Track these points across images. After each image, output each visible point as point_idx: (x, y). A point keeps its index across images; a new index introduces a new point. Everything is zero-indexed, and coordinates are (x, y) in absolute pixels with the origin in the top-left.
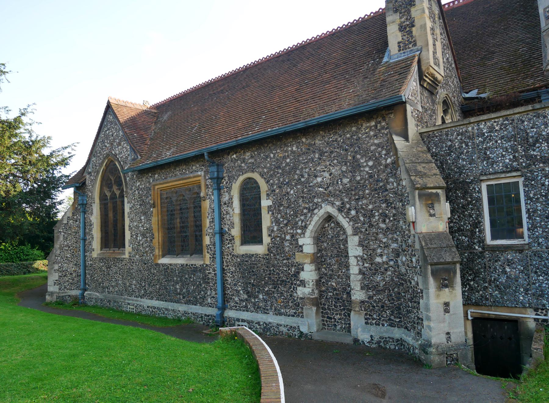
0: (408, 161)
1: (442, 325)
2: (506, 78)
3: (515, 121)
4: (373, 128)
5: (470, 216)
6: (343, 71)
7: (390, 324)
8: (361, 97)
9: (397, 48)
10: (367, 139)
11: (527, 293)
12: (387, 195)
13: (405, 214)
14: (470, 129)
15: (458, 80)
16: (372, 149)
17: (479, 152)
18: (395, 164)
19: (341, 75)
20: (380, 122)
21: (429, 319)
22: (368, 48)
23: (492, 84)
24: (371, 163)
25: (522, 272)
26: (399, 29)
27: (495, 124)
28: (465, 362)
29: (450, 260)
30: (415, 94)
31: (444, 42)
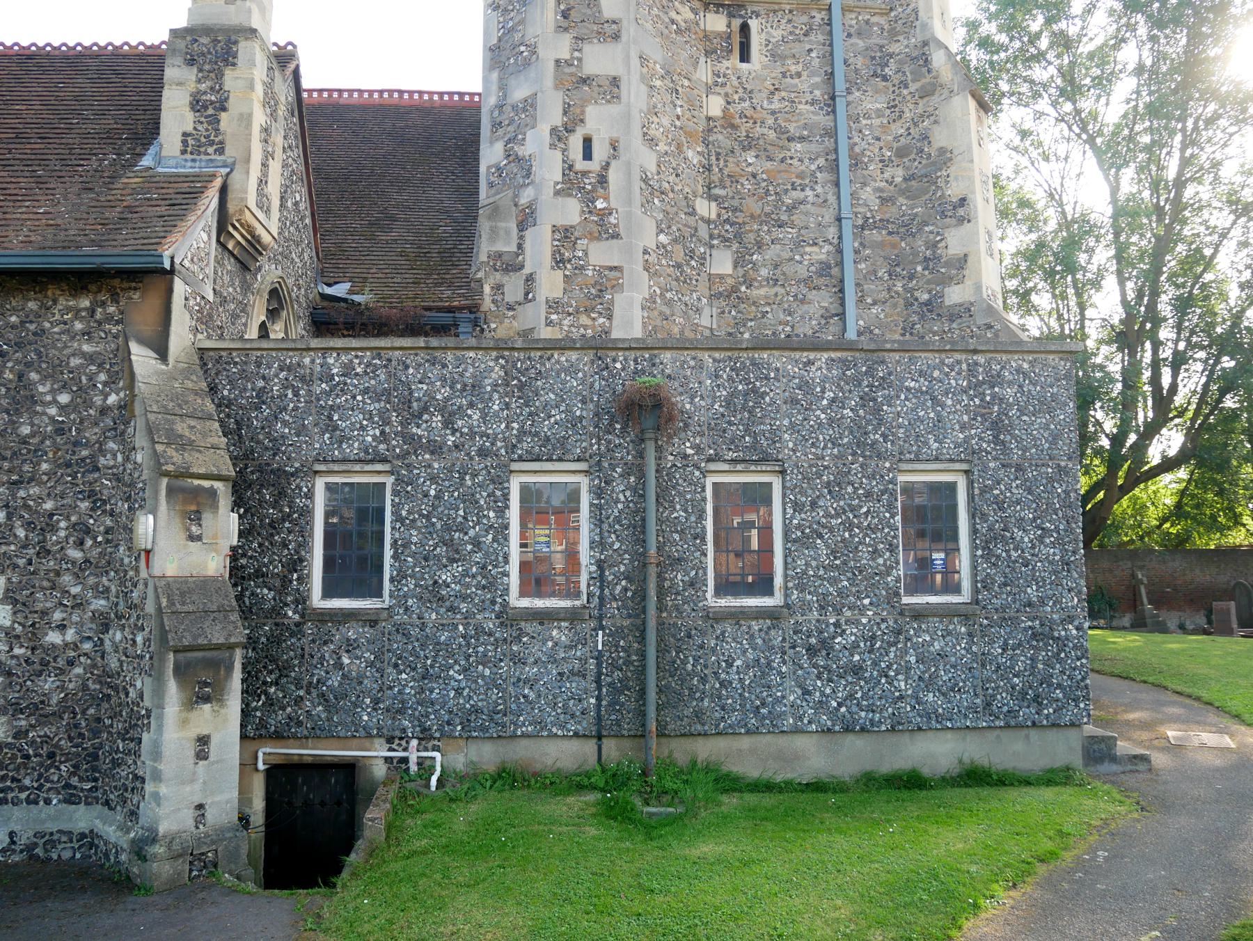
0: (155, 408)
1: (188, 789)
2: (407, 276)
3: (393, 362)
4: (83, 314)
5: (285, 545)
6: (33, 157)
7: (68, 797)
8: (63, 233)
9: (178, 146)
10: (64, 338)
11: (377, 707)
12: (96, 481)
13: (131, 530)
14: (307, 361)
15: (314, 254)
16: (72, 364)
17: (319, 413)
18: (126, 407)
19: (25, 163)
20: (103, 304)
21: (157, 776)
22: (113, 122)
23: (380, 280)
24: (64, 398)
25: (372, 664)
26: (191, 103)
27: (357, 361)
28: (233, 866)
29: (222, 640)
30: (201, 260)
31: (295, 166)
